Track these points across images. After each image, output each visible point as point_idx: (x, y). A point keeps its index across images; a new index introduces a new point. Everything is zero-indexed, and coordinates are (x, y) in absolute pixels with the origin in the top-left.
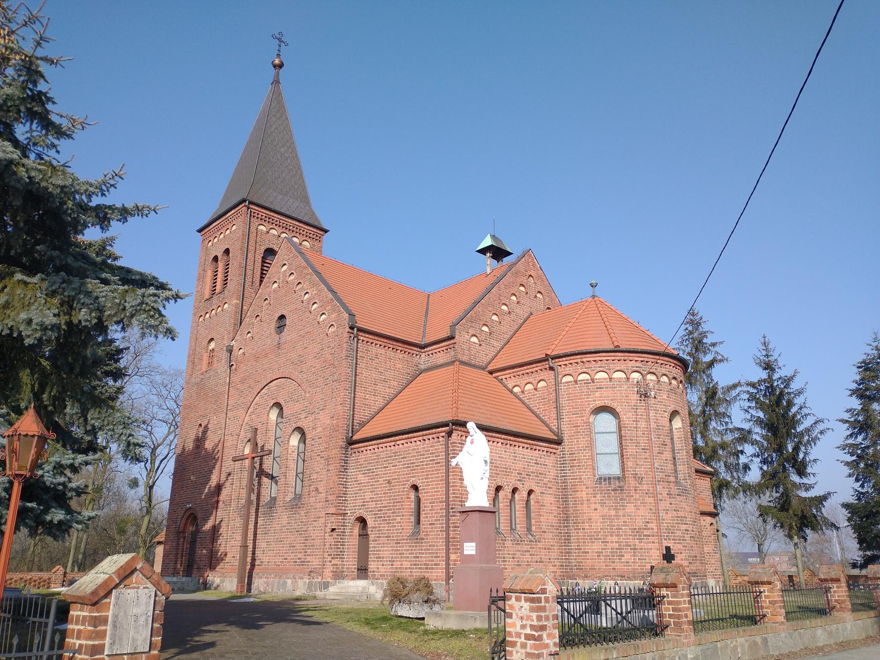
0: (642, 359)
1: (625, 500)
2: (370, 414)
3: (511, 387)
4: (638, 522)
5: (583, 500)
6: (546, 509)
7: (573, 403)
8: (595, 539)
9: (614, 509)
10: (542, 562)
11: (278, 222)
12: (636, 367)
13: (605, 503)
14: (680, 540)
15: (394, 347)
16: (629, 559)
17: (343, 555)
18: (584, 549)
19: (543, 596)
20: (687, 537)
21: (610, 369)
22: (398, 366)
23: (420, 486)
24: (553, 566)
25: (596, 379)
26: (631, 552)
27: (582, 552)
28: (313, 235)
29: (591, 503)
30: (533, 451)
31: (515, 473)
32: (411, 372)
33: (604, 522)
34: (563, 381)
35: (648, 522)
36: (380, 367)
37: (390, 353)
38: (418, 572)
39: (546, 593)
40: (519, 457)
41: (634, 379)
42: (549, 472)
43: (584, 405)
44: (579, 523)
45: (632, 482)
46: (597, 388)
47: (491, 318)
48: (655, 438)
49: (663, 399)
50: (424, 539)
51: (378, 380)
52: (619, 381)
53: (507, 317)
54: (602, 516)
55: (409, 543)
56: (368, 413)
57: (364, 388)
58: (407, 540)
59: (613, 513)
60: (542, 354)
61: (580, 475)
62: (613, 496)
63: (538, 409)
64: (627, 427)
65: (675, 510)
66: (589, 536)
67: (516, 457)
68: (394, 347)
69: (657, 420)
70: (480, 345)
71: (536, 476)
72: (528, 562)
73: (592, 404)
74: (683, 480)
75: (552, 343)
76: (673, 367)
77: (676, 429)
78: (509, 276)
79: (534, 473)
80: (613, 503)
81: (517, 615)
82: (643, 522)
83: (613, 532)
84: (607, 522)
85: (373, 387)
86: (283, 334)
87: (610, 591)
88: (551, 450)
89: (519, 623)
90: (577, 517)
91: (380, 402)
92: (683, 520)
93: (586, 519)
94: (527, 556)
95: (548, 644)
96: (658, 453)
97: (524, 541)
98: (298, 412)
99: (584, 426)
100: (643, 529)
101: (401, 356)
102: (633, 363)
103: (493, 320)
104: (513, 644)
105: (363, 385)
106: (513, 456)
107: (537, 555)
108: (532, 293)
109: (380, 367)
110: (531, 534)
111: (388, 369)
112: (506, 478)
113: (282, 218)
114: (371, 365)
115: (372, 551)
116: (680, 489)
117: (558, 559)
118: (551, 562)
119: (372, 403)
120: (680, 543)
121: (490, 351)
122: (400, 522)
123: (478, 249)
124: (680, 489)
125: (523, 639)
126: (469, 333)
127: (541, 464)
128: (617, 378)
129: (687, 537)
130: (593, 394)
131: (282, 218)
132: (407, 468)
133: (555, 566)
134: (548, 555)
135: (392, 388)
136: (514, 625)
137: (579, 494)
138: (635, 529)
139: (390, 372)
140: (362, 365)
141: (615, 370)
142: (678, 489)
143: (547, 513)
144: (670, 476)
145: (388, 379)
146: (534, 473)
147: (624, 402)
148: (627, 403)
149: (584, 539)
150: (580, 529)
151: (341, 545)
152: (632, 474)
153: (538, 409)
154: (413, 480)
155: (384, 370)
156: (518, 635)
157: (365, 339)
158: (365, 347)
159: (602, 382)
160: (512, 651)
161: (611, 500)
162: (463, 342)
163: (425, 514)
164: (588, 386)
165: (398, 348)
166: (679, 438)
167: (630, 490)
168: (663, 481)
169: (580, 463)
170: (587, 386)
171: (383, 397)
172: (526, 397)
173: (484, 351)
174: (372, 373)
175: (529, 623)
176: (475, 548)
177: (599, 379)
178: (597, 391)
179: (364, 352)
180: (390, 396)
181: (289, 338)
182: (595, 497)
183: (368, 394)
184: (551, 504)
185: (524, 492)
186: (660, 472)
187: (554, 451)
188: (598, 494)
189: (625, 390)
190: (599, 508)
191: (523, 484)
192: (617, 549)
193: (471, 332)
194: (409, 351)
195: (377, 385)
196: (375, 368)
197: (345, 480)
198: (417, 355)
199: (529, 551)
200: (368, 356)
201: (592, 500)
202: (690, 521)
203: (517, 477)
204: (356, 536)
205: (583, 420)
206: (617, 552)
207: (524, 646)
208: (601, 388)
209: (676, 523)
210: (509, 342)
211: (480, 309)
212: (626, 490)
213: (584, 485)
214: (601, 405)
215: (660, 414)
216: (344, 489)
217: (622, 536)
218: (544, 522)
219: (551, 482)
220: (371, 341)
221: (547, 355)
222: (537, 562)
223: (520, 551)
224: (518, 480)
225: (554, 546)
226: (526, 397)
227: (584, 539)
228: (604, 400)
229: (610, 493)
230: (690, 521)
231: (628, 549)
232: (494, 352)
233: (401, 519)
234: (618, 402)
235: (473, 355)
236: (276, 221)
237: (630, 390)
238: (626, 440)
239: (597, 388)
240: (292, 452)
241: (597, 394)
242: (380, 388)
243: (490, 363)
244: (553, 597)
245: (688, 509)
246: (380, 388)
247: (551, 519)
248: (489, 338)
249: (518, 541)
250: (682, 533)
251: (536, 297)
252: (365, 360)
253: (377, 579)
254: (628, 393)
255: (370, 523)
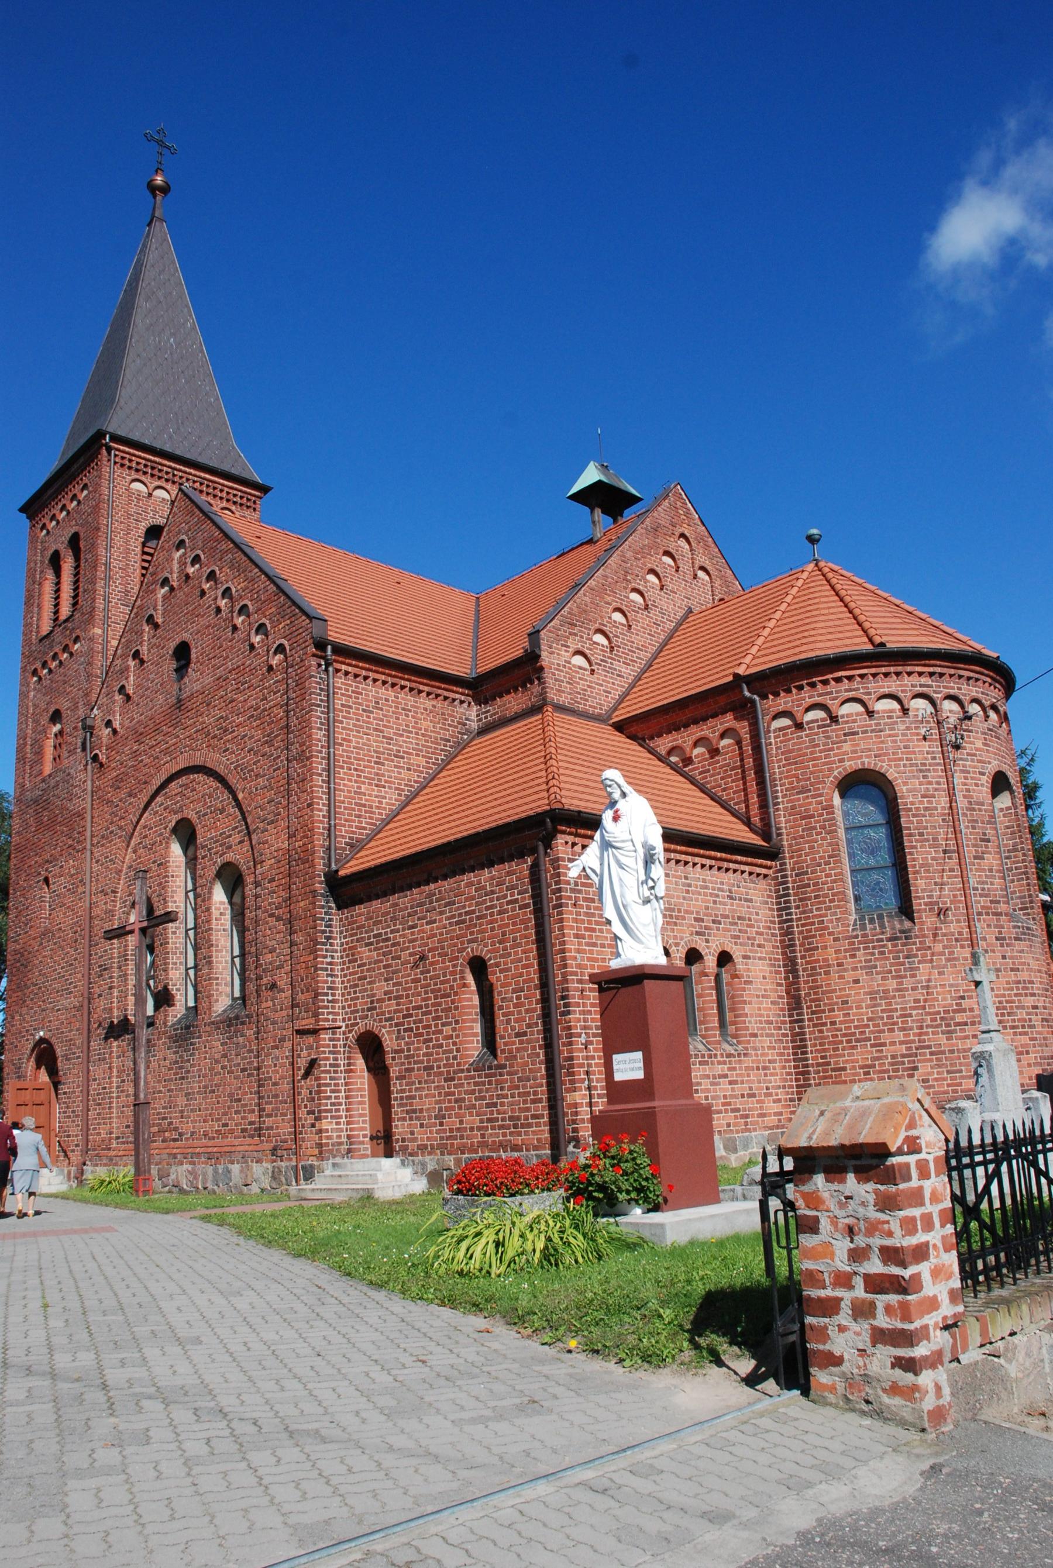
0: (931, 669)
1: (916, 956)
2: (371, 824)
3: (663, 753)
4: (944, 999)
5: (829, 966)
6: (755, 989)
7: (796, 769)
8: (857, 1041)
9: (893, 978)
10: (753, 1095)
11: (170, 476)
12: (921, 686)
13: (875, 967)
14: (1023, 1027)
15: (414, 685)
16: (929, 1074)
17: (337, 1110)
18: (836, 1063)
19: (912, 1159)
20: (1036, 1020)
21: (869, 694)
22: (424, 724)
23: (490, 959)
24: (775, 1101)
25: (843, 716)
26: (931, 1060)
27: (833, 1070)
28: (241, 498)
29: (846, 970)
30: (722, 874)
31: (690, 919)
32: (452, 736)
33: (875, 1006)
34: (772, 728)
35: (963, 998)
36: (384, 726)
37: (407, 699)
38: (498, 1136)
39: (918, 1151)
40: (696, 886)
41: (918, 709)
42: (757, 914)
43: (821, 771)
44: (824, 1011)
45: (926, 919)
46: (845, 735)
47: (610, 618)
48: (967, 827)
49: (977, 749)
50: (504, 1066)
51: (383, 753)
52: (890, 717)
53: (642, 616)
54: (870, 993)
55: (473, 1077)
56: (367, 823)
57: (356, 770)
58: (469, 1070)
59: (892, 984)
60: (726, 676)
61: (821, 916)
62: (890, 952)
63: (724, 790)
64: (910, 810)
65: (1012, 970)
66: (844, 1035)
67: (690, 885)
68: (414, 685)
69: (968, 790)
70: (593, 672)
71: (731, 924)
72: (725, 1097)
73: (837, 768)
74: (1021, 909)
75: (738, 662)
76: (990, 685)
77: (1001, 810)
78: (641, 534)
79: (727, 917)
80: (892, 965)
81: (834, 1220)
82: (953, 999)
83: (895, 1024)
84: (880, 1005)
85: (373, 768)
86: (186, 680)
87: (994, 1137)
88: (758, 870)
89: (842, 1246)
90: (819, 1000)
91: (391, 799)
92: (1027, 988)
93: (837, 1003)
94: (724, 1084)
95: (935, 1297)
96: (975, 858)
97: (715, 1056)
98: (224, 833)
99: (822, 814)
100: (954, 1011)
101: (429, 703)
102: (915, 679)
103: (615, 622)
104: (830, 1307)
105: (352, 764)
106: (684, 885)
107: (742, 1082)
108: (685, 567)
109: (384, 726)
110: (728, 1042)
111: (403, 730)
112: (673, 930)
113: (178, 467)
114: (368, 722)
115: (396, 1099)
116: (1019, 927)
117: (784, 1087)
118: (770, 1095)
119: (374, 801)
120: (1026, 1033)
121: (613, 684)
122: (451, 1037)
123: (575, 489)
124: (1019, 927)
125: (860, 1291)
126: (568, 647)
127: (740, 899)
128: (884, 711)
129: (1036, 1020)
130: (838, 748)
131: (178, 467)
132: (457, 923)
133: (779, 1100)
134: (765, 1082)
135: (415, 771)
136: (826, 1250)
137: (817, 955)
138: (939, 1013)
139: (408, 737)
140: (348, 724)
141: (878, 695)
142: (1015, 927)
143: (758, 996)
144: (998, 902)
145: (404, 752)
146: (727, 917)
147: (901, 759)
148: (907, 759)
149: (835, 1043)
150: (825, 1024)
151: (332, 1091)
152: (926, 904)
153: (724, 790)
154: (472, 950)
155: (395, 734)
156: (844, 1280)
157: (350, 669)
158: (351, 686)
159: (855, 721)
160: (826, 1328)
161: (887, 959)
162: (558, 665)
163: (504, 1015)
164: (827, 732)
165: (421, 687)
166: (1007, 827)
167: (924, 936)
168: (987, 914)
169: (819, 890)
170: (823, 732)
171: (396, 789)
172: (697, 768)
173: (602, 685)
174: (369, 740)
175: (877, 1242)
176: (641, 1064)
177: (848, 716)
178: (845, 741)
179: (351, 697)
180: (411, 786)
181: (197, 686)
182: (853, 956)
183: (364, 783)
184: (764, 978)
185: (711, 957)
186: (981, 896)
187: (764, 871)
188: (859, 949)
189: (903, 735)
190: (864, 978)
191: (707, 941)
192: (903, 1056)
193: (574, 644)
194: (446, 694)
195: (383, 764)
196: (376, 730)
197: (329, 960)
198: (462, 702)
199: (725, 1076)
200: (360, 704)
201: (848, 963)
202: (1038, 989)
203: (692, 926)
204: (362, 1071)
205: (821, 803)
206: (903, 1063)
207: (863, 1311)
208: (854, 734)
209: (1016, 995)
210: (651, 666)
211: (587, 599)
212: (917, 937)
213: (830, 934)
214: (855, 768)
215: (972, 778)
216: (330, 979)
217: (911, 1029)
218: (752, 1016)
219: (761, 934)
220: (364, 673)
221: (736, 676)
222: (743, 1096)
223: (708, 1077)
224: (697, 933)
225: (774, 1061)
226: (697, 768)
227: (835, 1043)
228: (861, 757)
229: (884, 946)
230: (1038, 989)
231: (924, 1054)
232: (623, 687)
233: (454, 1030)
234: (890, 760)
235: (579, 693)
236: (167, 473)
237: (912, 734)
238: (911, 835)
239: (845, 735)
240: (221, 914)
241: (847, 747)
242: (389, 768)
243: (615, 709)
244: (936, 1160)
245: (1034, 964)
246: (389, 768)
247: (765, 1009)
248: (609, 658)
249: (703, 1056)
250: (1028, 1014)
251: (695, 576)
252: (354, 713)
253: (411, 1155)
254: (908, 740)
255: (389, 1042)
